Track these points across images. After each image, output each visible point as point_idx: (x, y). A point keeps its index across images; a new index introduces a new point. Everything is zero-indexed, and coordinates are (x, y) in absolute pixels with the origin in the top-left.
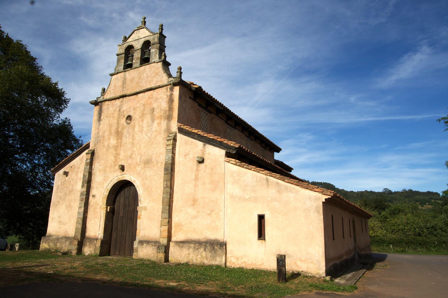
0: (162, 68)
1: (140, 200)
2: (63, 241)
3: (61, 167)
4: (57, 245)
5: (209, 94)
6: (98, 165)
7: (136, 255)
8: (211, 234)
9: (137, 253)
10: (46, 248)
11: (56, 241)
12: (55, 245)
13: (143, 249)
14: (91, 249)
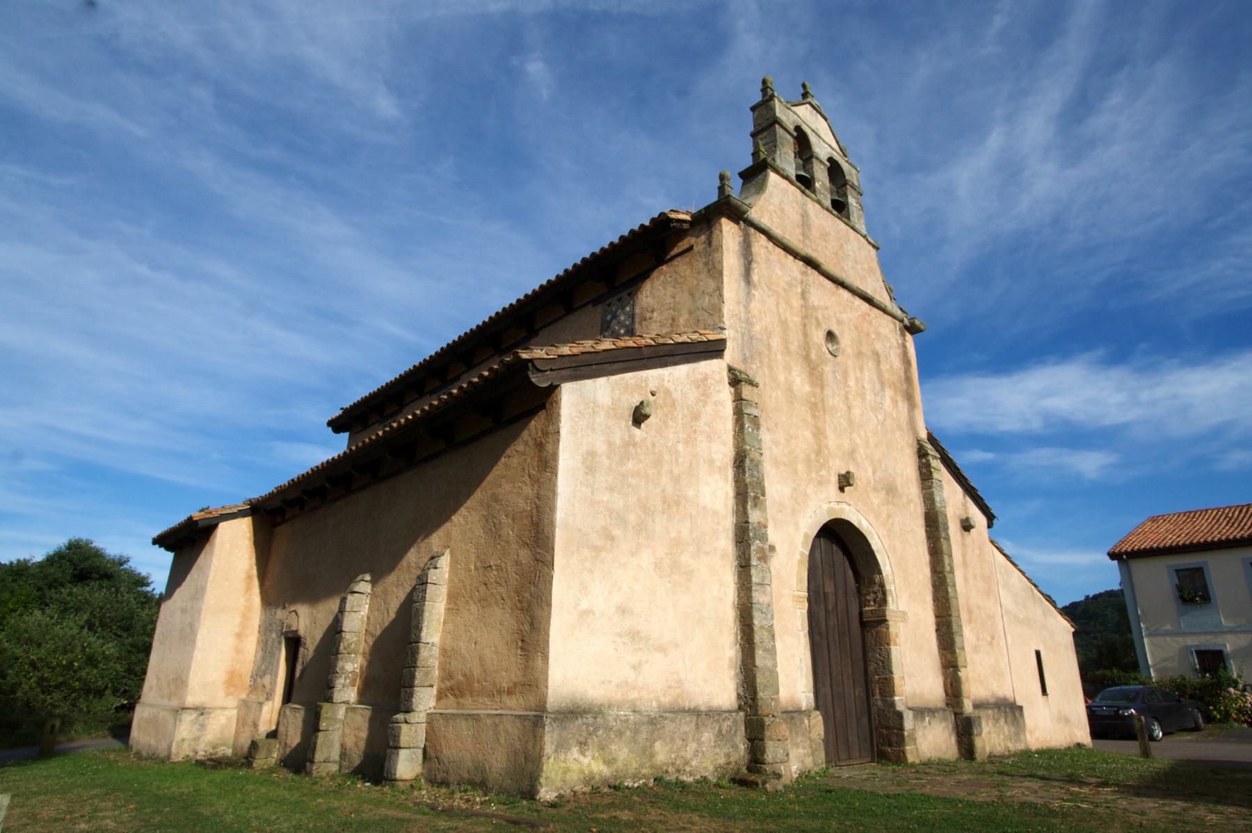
0: (866, 293)
1: (890, 590)
2: (686, 728)
3: (592, 365)
4: (652, 755)
7: (915, 752)
8: (993, 638)
9: (915, 744)
10: (593, 778)
11: (643, 735)
12: (644, 753)
13: (926, 732)
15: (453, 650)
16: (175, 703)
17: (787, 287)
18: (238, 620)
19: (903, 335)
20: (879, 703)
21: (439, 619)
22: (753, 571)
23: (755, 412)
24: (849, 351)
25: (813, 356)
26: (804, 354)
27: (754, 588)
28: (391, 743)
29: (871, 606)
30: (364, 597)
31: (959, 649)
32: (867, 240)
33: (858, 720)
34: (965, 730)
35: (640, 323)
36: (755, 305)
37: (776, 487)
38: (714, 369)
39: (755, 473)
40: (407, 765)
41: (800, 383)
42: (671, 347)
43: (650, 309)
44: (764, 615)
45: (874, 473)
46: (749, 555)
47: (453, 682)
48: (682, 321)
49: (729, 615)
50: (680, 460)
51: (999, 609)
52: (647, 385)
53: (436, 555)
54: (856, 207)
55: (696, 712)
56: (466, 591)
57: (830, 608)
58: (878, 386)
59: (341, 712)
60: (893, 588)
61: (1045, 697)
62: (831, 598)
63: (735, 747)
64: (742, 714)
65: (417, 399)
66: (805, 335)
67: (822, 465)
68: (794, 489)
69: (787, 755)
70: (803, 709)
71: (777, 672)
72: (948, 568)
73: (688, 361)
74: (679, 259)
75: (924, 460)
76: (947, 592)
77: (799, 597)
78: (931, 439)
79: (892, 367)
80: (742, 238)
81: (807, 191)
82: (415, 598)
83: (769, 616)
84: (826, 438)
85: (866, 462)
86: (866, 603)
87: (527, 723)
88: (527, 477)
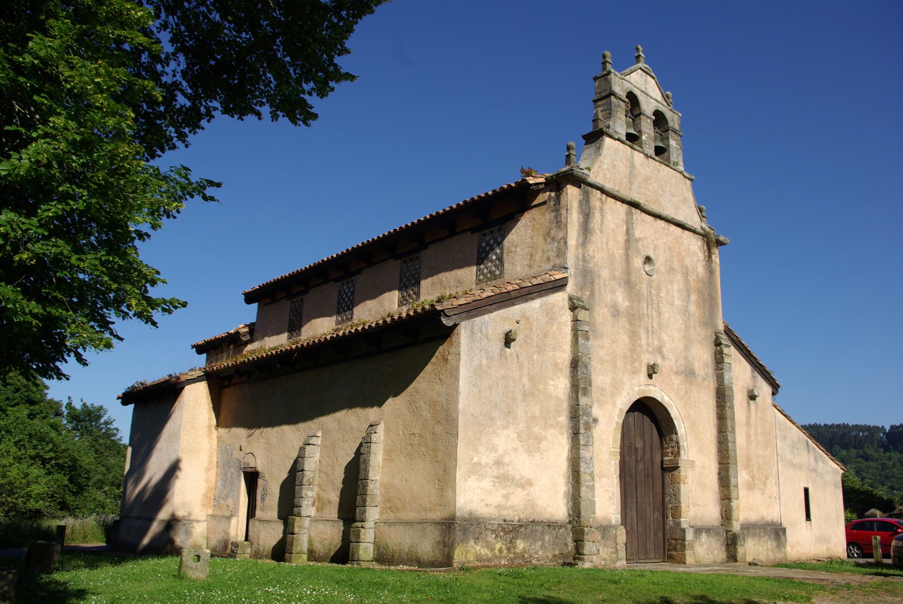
1: (683, 446)
20: (671, 523)
21: (379, 466)
22: (581, 437)
23: (587, 328)
24: (663, 269)
27: (581, 448)
29: (670, 456)
30: (316, 447)
31: (733, 486)
32: (683, 175)
33: (655, 534)
34: (731, 543)
35: (508, 254)
37: (600, 377)
38: (559, 299)
39: (585, 372)
40: (366, 549)
41: (621, 299)
42: (530, 288)
44: (587, 465)
46: (579, 427)
48: (537, 258)
53: (373, 424)
54: (676, 148)
56: (397, 448)
59: (307, 523)
60: (685, 444)
61: (809, 522)
62: (640, 452)
63: (566, 545)
65: (322, 284)
68: (614, 378)
71: (595, 501)
72: (730, 429)
73: (541, 296)
74: (536, 209)
75: (718, 348)
76: (728, 446)
78: (728, 332)
79: (698, 277)
81: (635, 146)
82: (362, 451)
83: (591, 466)
84: (640, 339)
86: (666, 454)
88: (438, 379)
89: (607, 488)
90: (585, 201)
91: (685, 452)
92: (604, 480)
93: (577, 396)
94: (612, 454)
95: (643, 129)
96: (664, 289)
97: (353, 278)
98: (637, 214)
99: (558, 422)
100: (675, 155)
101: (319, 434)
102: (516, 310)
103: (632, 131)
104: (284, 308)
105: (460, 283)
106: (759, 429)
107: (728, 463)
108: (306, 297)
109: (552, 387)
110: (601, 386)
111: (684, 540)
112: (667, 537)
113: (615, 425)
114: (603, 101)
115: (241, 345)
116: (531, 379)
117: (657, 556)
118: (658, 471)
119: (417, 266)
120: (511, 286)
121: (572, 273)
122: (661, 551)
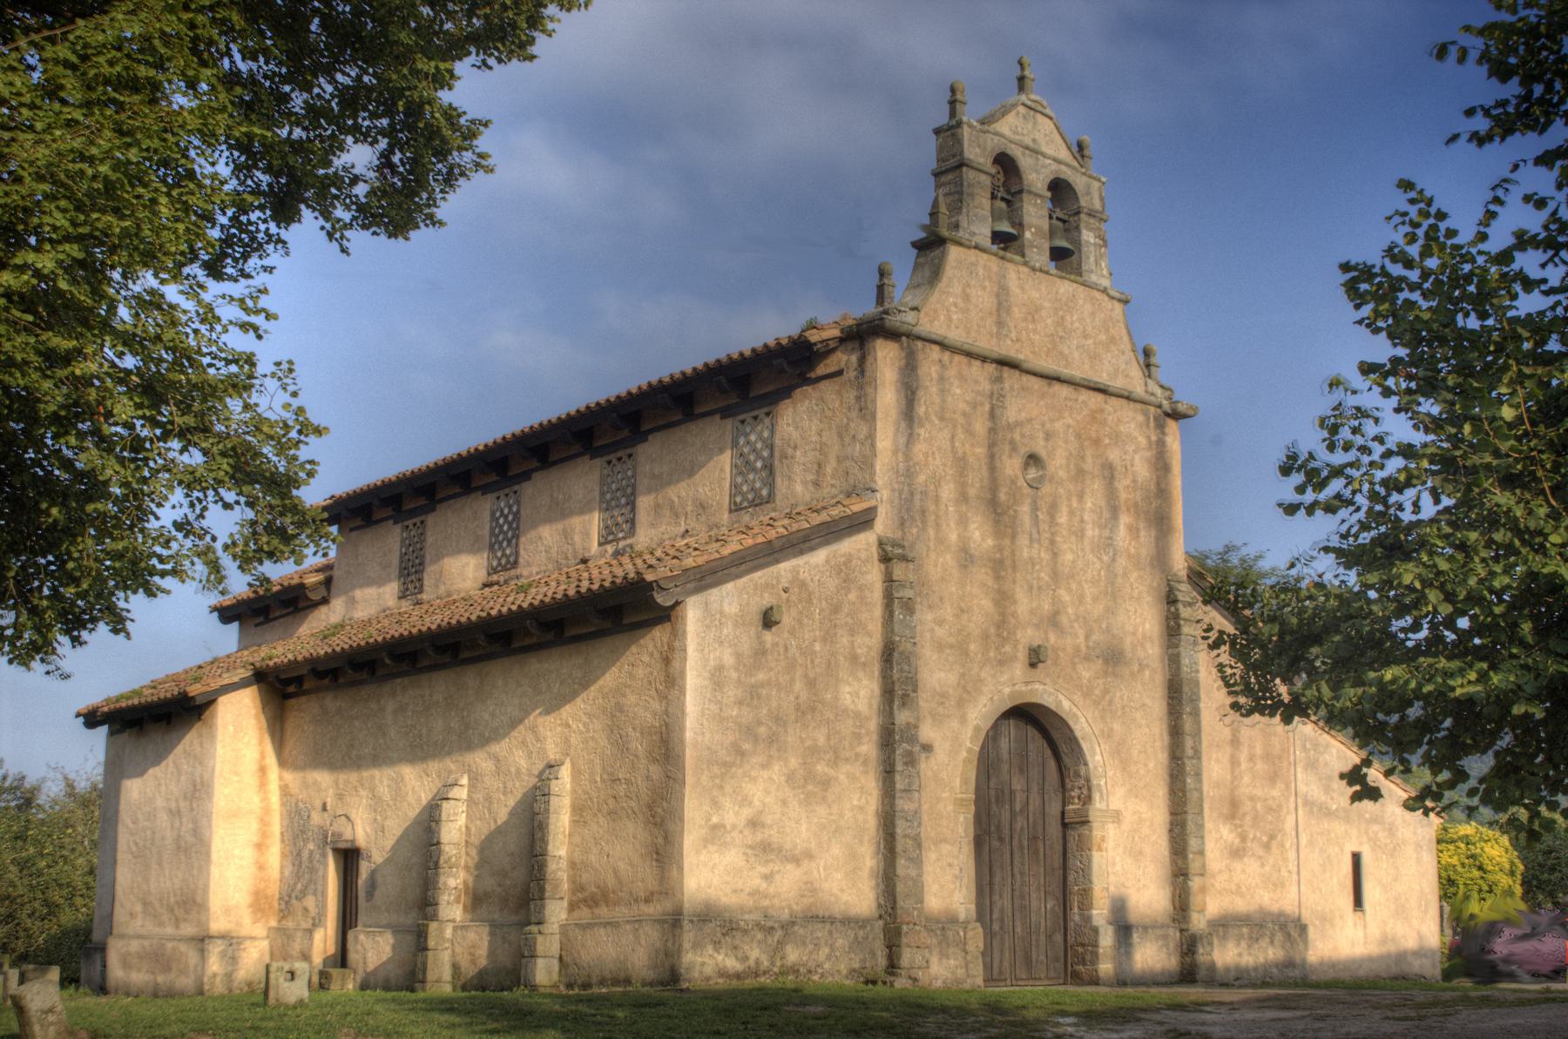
1: (1099, 785)
5: (750, 348)
6: (930, 617)
8: (1272, 837)
14: (952, 962)
15: (582, 862)
16: (188, 930)
17: (968, 409)
18: (255, 826)
19: (1161, 427)
20: (1077, 918)
22: (898, 777)
23: (908, 593)
25: (1002, 497)
26: (989, 496)
27: (898, 795)
28: (526, 954)
31: (1194, 853)
32: (1108, 295)
33: (1049, 937)
36: (919, 448)
38: (861, 544)
41: (980, 535)
43: (792, 444)
45: (1087, 637)
47: (586, 894)
48: (829, 470)
49: (871, 822)
50: (817, 661)
51: (1292, 799)
52: (779, 582)
53: (553, 763)
54: (1095, 244)
55: (832, 920)
57: (1018, 809)
58: (1106, 515)
60: (1102, 783)
61: (1359, 914)
62: (1019, 799)
64: (881, 923)
66: (992, 469)
67: (1006, 640)
68: (963, 675)
69: (927, 962)
70: (961, 919)
72: (1189, 752)
75: (1173, 609)
77: (962, 800)
79: (1134, 481)
80: (904, 362)
81: (1009, 255)
83: (916, 824)
84: (1015, 602)
85: (1076, 624)
87: (666, 926)
89: (951, 860)
90: (909, 369)
91: (1101, 795)
92: (946, 848)
93: (891, 709)
94: (960, 803)
95: (1027, 220)
96: (1064, 510)
97: (516, 488)
98: (1011, 378)
99: (857, 755)
100: (1092, 259)
101: (465, 781)
102: (785, 568)
103: (1005, 227)
104: (390, 540)
105: (703, 508)
106: (1259, 751)
107: (1186, 812)
108: (430, 519)
109: (848, 696)
110: (938, 689)
111: (1096, 945)
112: (1071, 940)
113: (965, 754)
114: (950, 176)
115: (304, 609)
116: (811, 684)
117: (1052, 974)
118: (1054, 829)
119: (629, 473)
120: (773, 532)
121: (885, 498)
122: (1060, 966)
